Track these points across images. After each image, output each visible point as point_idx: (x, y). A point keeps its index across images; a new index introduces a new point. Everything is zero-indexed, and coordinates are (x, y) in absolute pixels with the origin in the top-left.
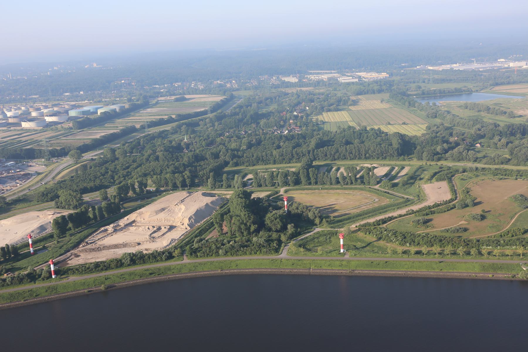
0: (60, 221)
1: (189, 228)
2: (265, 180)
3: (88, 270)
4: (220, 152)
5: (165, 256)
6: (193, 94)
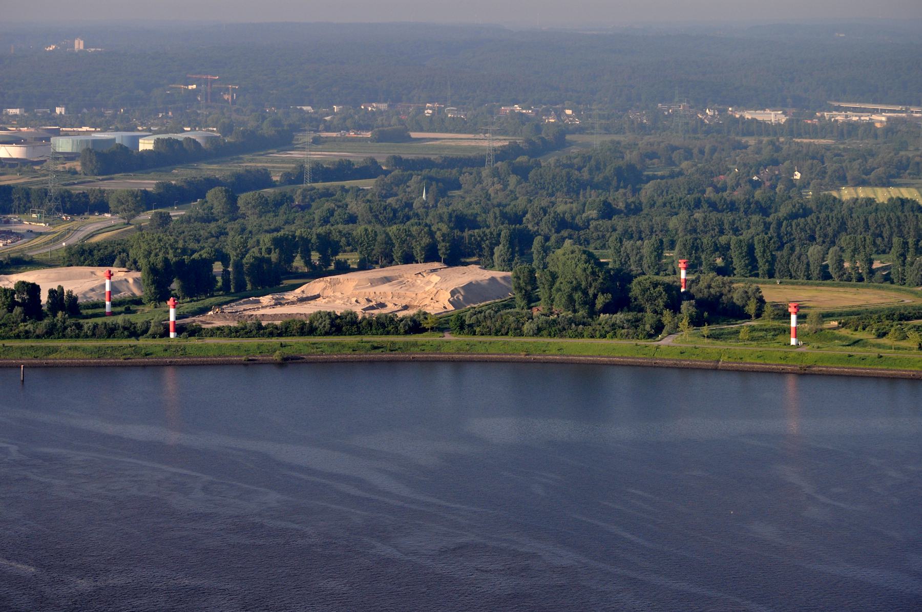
2: (641, 259)
4: (525, 213)
5: (405, 326)
6: (434, 131)
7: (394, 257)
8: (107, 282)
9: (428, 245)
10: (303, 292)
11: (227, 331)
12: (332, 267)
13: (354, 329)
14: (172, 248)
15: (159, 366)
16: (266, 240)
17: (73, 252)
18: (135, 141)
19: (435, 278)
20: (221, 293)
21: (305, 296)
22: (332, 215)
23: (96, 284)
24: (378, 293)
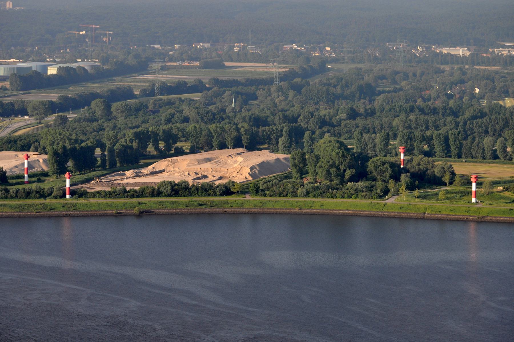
0: (59, 151)
2: (375, 146)
3: (113, 195)
4: (299, 116)
5: (220, 190)
6: (240, 61)
7: (214, 144)
8: (26, 162)
9: (235, 137)
10: (154, 168)
11: (103, 194)
12: (173, 151)
13: (187, 192)
14: (68, 139)
15: (59, 217)
17: (4, 141)
19: (240, 159)
20: (100, 168)
21: (155, 170)
22: (173, 117)
23: (19, 162)
24: (202, 169)
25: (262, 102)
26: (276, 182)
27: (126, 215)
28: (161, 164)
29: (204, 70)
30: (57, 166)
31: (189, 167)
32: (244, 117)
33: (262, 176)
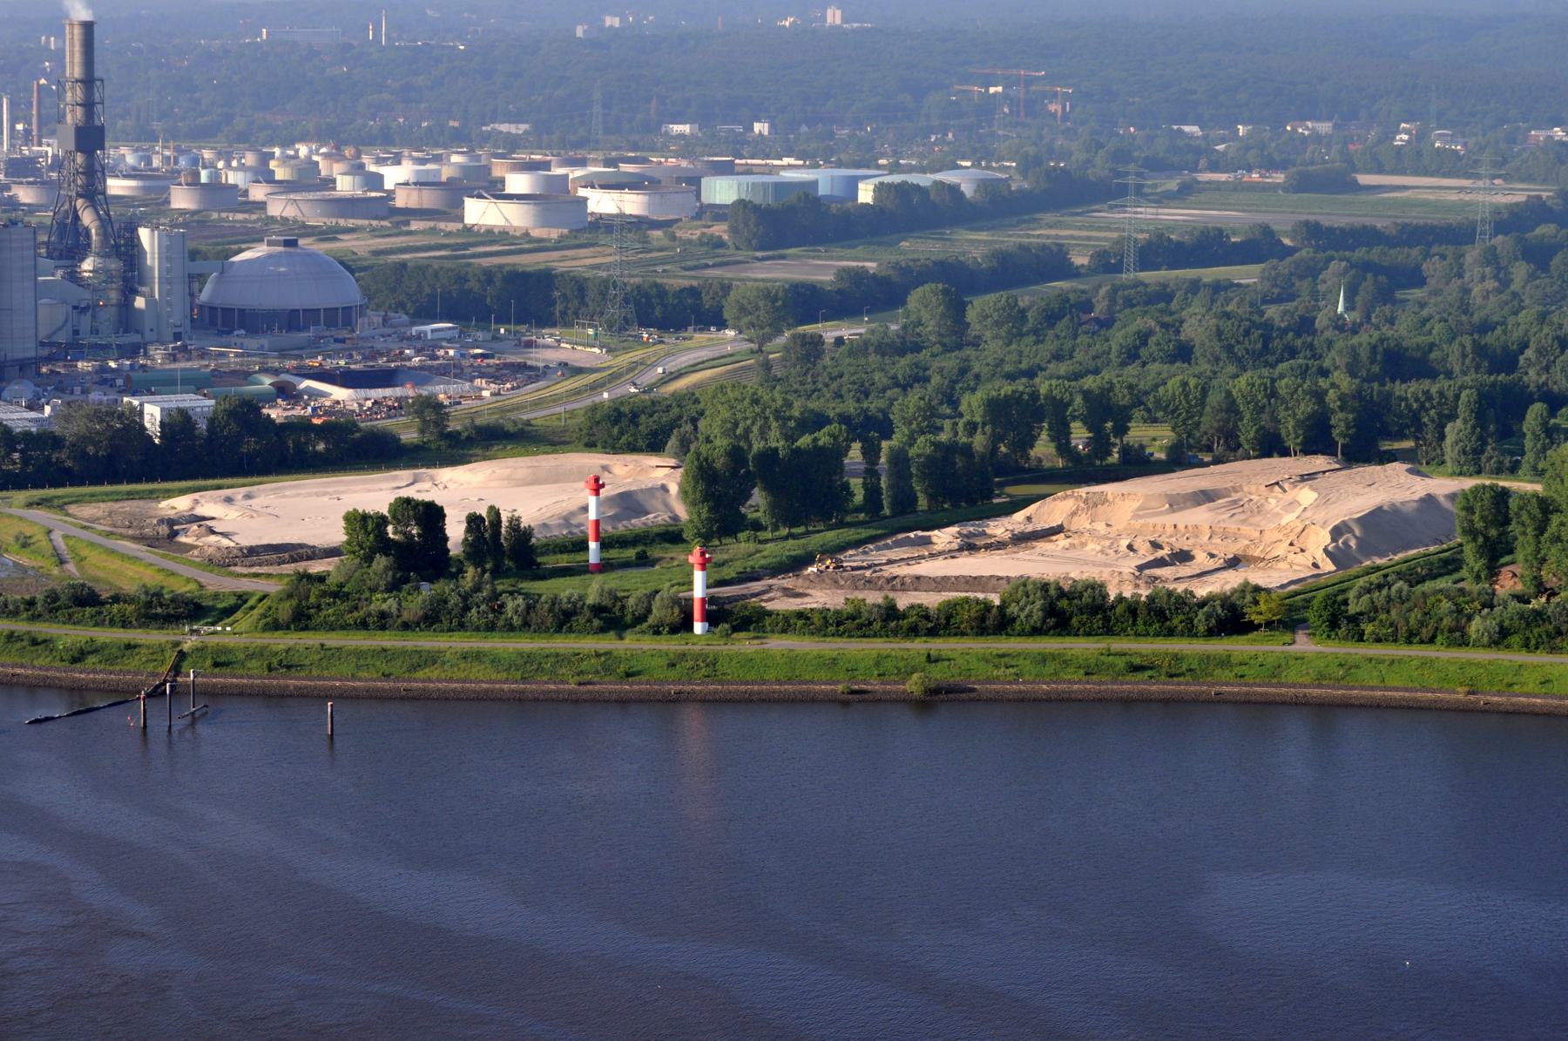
0: (719, 465)
1: (1328, 566)
4: (1524, 346)
5: (1208, 616)
6: (1403, 172)
7: (1242, 439)
9: (1310, 417)
10: (1029, 519)
12: (1115, 457)
13: (1097, 621)
14: (777, 419)
16: (975, 404)
17: (598, 417)
18: (852, 185)
19: (1306, 495)
20: (862, 516)
21: (1030, 528)
22: (1145, 343)
24: (1181, 527)
25: (1436, 293)
26: (1400, 591)
27: (879, 701)
28: (1056, 508)
29: (1296, 197)
30: (710, 511)
31: (1141, 521)
32: (1353, 348)
33: (1368, 556)
